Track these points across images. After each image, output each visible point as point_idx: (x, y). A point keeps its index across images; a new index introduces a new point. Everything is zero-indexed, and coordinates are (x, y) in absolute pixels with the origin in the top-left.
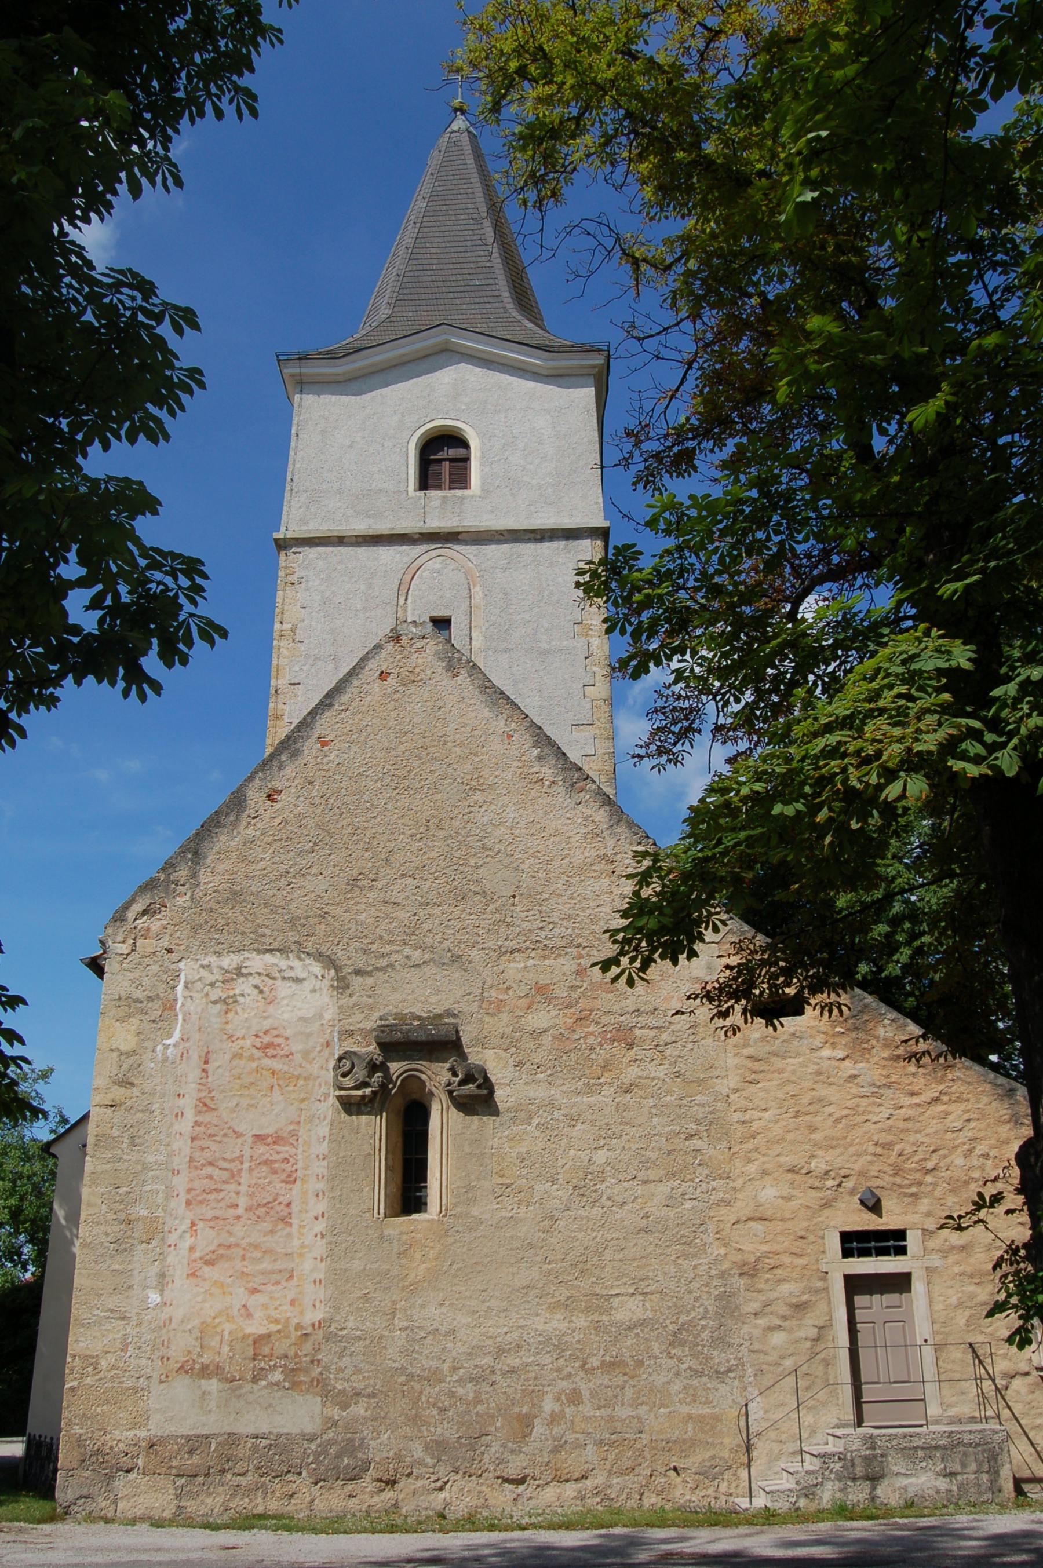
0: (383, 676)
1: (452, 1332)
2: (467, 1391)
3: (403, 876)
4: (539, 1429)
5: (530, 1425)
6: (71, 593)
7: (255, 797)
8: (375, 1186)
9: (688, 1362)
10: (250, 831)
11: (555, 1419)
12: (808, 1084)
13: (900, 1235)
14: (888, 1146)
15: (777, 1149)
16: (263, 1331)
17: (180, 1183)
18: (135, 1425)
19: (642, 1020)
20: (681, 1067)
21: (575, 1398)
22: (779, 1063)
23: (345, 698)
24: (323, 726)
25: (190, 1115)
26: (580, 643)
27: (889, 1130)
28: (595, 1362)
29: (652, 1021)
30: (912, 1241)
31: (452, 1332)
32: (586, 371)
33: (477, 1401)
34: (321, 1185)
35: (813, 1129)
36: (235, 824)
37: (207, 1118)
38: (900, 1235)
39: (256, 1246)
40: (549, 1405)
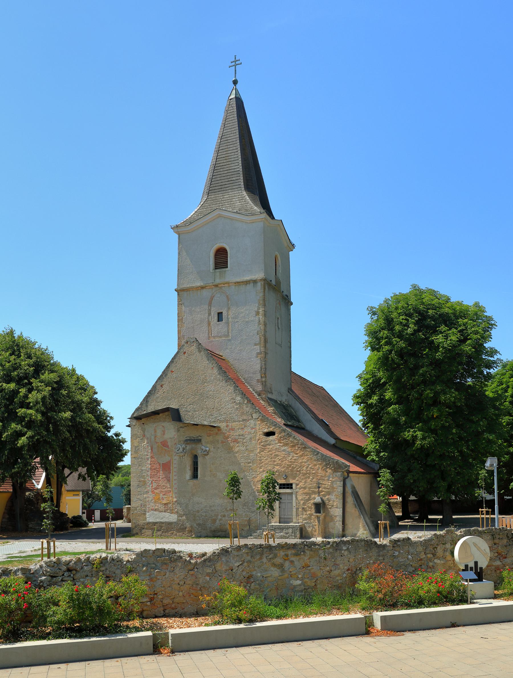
0: (185, 353)
1: (201, 503)
2: (204, 514)
3: (190, 404)
4: (218, 521)
5: (216, 521)
6: (62, 510)
7: (158, 387)
8: (188, 474)
9: (247, 509)
10: (158, 395)
11: (221, 520)
12: (274, 451)
13: (292, 484)
14: (290, 466)
15: (267, 466)
16: (166, 502)
17: (149, 473)
18: (144, 520)
19: (240, 437)
20: (248, 447)
21: (224, 516)
22: (268, 447)
23: (176, 360)
24: (172, 368)
25: (150, 460)
26: (257, 318)
27: (291, 462)
28: (228, 509)
29: (242, 437)
30: (294, 486)
31: (201, 503)
32: (260, 220)
33: (206, 516)
34: (175, 474)
35: (274, 461)
36: (154, 394)
37: (153, 460)
38: (292, 484)
39: (164, 486)
40: (219, 517)
